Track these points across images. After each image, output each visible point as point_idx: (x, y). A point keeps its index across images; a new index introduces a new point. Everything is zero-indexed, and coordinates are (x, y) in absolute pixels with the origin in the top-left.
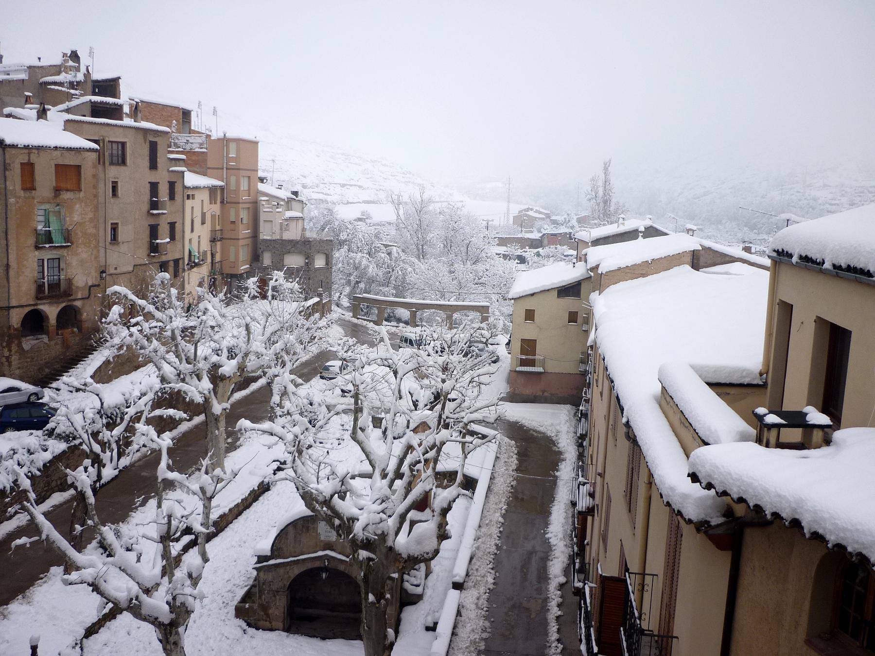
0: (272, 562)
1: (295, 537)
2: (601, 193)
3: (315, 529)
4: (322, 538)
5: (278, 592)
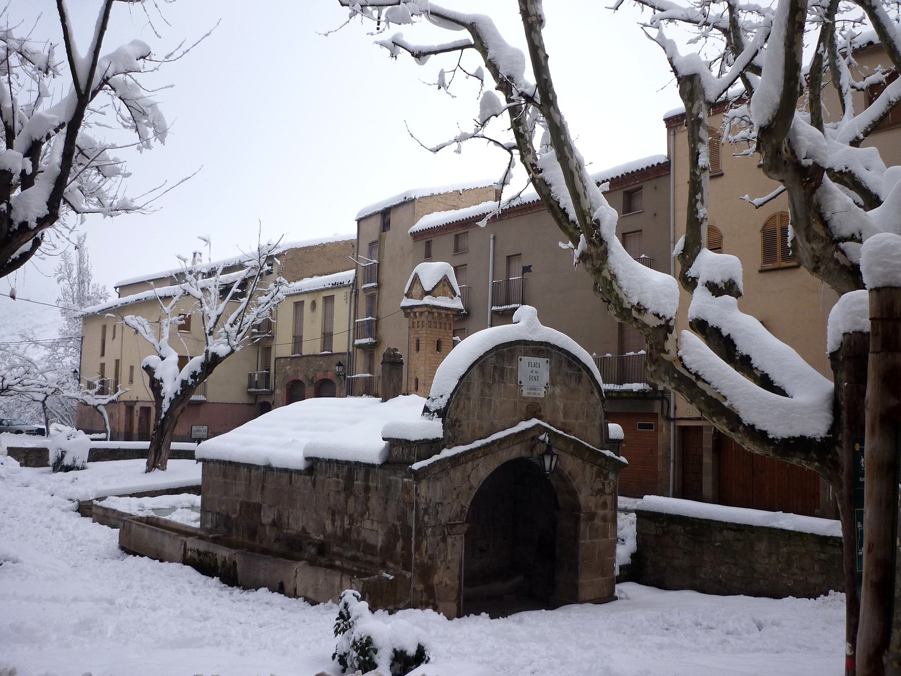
0: (446, 453)
1: (482, 391)
2: (75, 274)
3: (514, 372)
4: (525, 394)
5: (452, 526)
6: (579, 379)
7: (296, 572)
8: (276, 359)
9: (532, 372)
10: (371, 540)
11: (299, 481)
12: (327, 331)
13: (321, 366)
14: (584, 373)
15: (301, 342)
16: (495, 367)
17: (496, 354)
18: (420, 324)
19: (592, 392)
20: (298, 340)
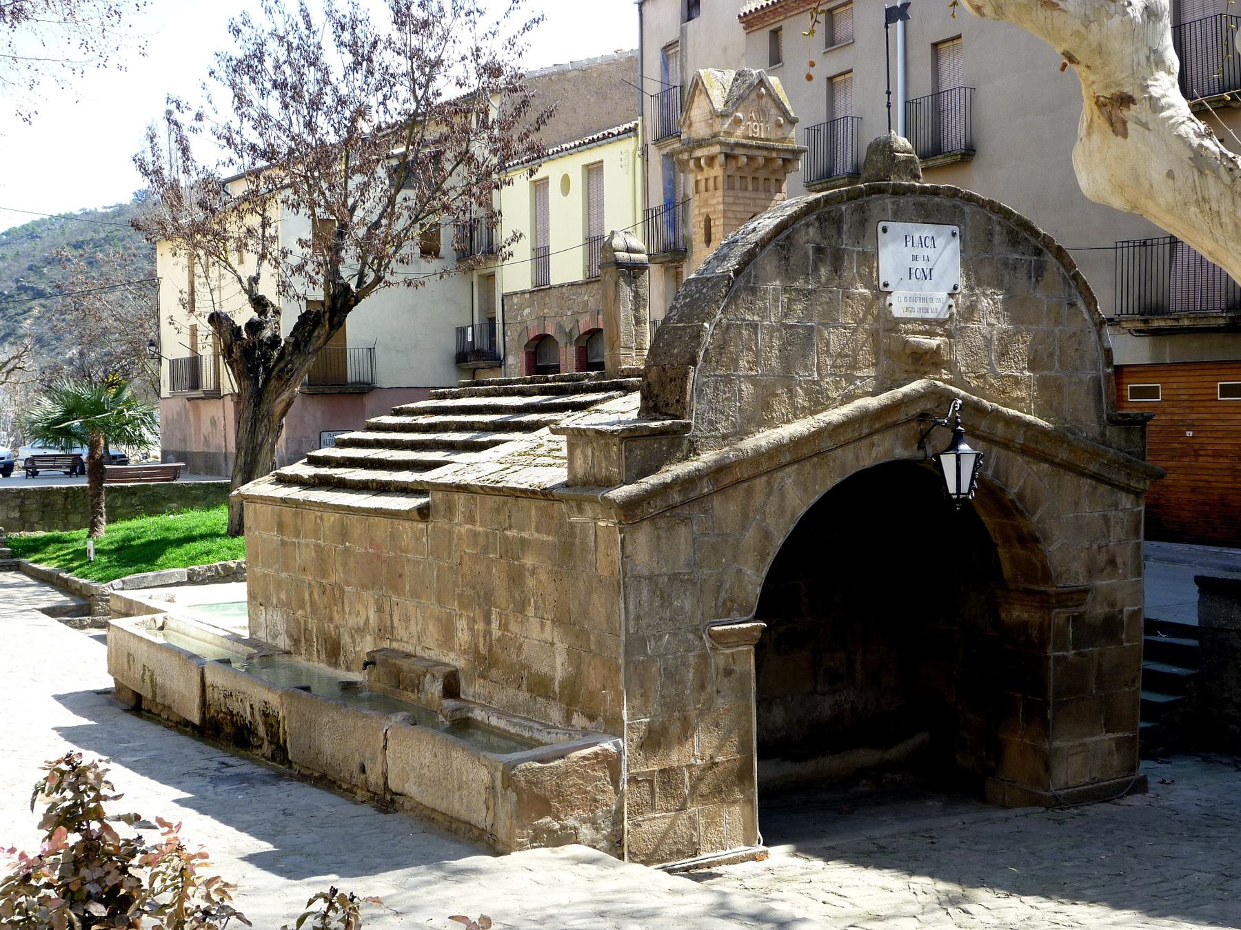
3: (870, 258)
6: (1038, 272)
7: (386, 739)
8: (504, 296)
9: (915, 258)
10: (541, 667)
11: (529, 528)
12: (594, 234)
13: (586, 303)
14: (1050, 258)
15: (547, 256)
16: (819, 250)
17: (818, 218)
18: (711, 182)
19: (1072, 305)
20: (541, 256)
